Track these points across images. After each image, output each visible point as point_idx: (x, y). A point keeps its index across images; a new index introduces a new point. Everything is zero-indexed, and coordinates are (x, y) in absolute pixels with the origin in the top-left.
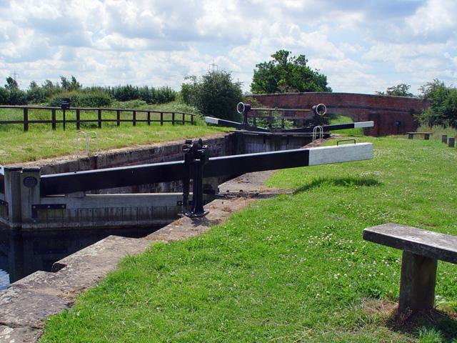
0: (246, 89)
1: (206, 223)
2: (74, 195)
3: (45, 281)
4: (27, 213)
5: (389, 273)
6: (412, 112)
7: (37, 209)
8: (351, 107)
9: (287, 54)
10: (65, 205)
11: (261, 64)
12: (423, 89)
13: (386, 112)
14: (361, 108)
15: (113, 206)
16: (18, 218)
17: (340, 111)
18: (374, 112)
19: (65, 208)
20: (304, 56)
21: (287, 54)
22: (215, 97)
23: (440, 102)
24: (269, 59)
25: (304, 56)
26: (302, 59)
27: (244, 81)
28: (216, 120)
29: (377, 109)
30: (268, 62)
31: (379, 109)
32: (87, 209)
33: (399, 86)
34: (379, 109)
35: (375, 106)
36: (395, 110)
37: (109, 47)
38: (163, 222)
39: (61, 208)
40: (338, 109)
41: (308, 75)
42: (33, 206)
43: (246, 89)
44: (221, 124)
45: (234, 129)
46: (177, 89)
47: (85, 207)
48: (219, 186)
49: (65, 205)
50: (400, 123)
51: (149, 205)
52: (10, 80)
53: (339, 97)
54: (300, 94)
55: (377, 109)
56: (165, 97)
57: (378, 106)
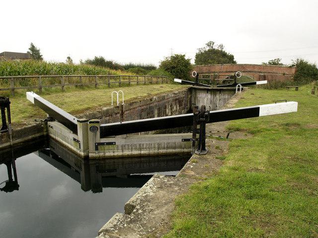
0: (193, 62)
1: (209, 153)
2: (120, 136)
3: (125, 225)
4: (92, 147)
7: (98, 146)
10: (115, 143)
14: (255, 72)
15: (144, 143)
16: (86, 149)
18: (262, 74)
19: (115, 144)
22: (176, 67)
27: (191, 57)
28: (180, 81)
32: (128, 145)
35: (263, 71)
37: (33, 102)
38: (91, 67)
39: (113, 144)
41: (224, 55)
42: (95, 144)
43: (193, 62)
44: (183, 83)
45: (191, 86)
46: (157, 65)
47: (127, 143)
48: (207, 124)
49: (115, 143)
51: (166, 141)
52: (69, 58)
56: (150, 68)
57: (265, 71)
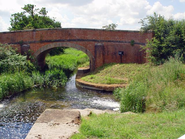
5: (78, 116)
6: (133, 43)
8: (79, 40)
9: (33, 7)
11: (16, 14)
12: (142, 22)
13: (109, 43)
17: (69, 44)
18: (99, 44)
20: (45, 9)
21: (33, 7)
23: (166, 33)
24: (20, 11)
25: (45, 9)
26: (44, 11)
29: (102, 41)
30: (20, 13)
31: (104, 41)
33: (110, 25)
34: (104, 41)
35: (99, 38)
36: (117, 42)
40: (68, 43)
50: (123, 53)
53: (68, 31)
54: (33, 31)
55: (102, 41)
57: (102, 38)
